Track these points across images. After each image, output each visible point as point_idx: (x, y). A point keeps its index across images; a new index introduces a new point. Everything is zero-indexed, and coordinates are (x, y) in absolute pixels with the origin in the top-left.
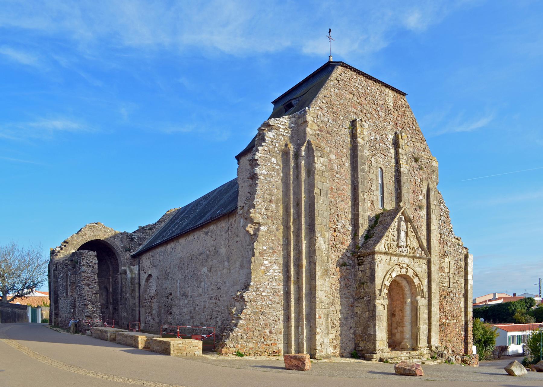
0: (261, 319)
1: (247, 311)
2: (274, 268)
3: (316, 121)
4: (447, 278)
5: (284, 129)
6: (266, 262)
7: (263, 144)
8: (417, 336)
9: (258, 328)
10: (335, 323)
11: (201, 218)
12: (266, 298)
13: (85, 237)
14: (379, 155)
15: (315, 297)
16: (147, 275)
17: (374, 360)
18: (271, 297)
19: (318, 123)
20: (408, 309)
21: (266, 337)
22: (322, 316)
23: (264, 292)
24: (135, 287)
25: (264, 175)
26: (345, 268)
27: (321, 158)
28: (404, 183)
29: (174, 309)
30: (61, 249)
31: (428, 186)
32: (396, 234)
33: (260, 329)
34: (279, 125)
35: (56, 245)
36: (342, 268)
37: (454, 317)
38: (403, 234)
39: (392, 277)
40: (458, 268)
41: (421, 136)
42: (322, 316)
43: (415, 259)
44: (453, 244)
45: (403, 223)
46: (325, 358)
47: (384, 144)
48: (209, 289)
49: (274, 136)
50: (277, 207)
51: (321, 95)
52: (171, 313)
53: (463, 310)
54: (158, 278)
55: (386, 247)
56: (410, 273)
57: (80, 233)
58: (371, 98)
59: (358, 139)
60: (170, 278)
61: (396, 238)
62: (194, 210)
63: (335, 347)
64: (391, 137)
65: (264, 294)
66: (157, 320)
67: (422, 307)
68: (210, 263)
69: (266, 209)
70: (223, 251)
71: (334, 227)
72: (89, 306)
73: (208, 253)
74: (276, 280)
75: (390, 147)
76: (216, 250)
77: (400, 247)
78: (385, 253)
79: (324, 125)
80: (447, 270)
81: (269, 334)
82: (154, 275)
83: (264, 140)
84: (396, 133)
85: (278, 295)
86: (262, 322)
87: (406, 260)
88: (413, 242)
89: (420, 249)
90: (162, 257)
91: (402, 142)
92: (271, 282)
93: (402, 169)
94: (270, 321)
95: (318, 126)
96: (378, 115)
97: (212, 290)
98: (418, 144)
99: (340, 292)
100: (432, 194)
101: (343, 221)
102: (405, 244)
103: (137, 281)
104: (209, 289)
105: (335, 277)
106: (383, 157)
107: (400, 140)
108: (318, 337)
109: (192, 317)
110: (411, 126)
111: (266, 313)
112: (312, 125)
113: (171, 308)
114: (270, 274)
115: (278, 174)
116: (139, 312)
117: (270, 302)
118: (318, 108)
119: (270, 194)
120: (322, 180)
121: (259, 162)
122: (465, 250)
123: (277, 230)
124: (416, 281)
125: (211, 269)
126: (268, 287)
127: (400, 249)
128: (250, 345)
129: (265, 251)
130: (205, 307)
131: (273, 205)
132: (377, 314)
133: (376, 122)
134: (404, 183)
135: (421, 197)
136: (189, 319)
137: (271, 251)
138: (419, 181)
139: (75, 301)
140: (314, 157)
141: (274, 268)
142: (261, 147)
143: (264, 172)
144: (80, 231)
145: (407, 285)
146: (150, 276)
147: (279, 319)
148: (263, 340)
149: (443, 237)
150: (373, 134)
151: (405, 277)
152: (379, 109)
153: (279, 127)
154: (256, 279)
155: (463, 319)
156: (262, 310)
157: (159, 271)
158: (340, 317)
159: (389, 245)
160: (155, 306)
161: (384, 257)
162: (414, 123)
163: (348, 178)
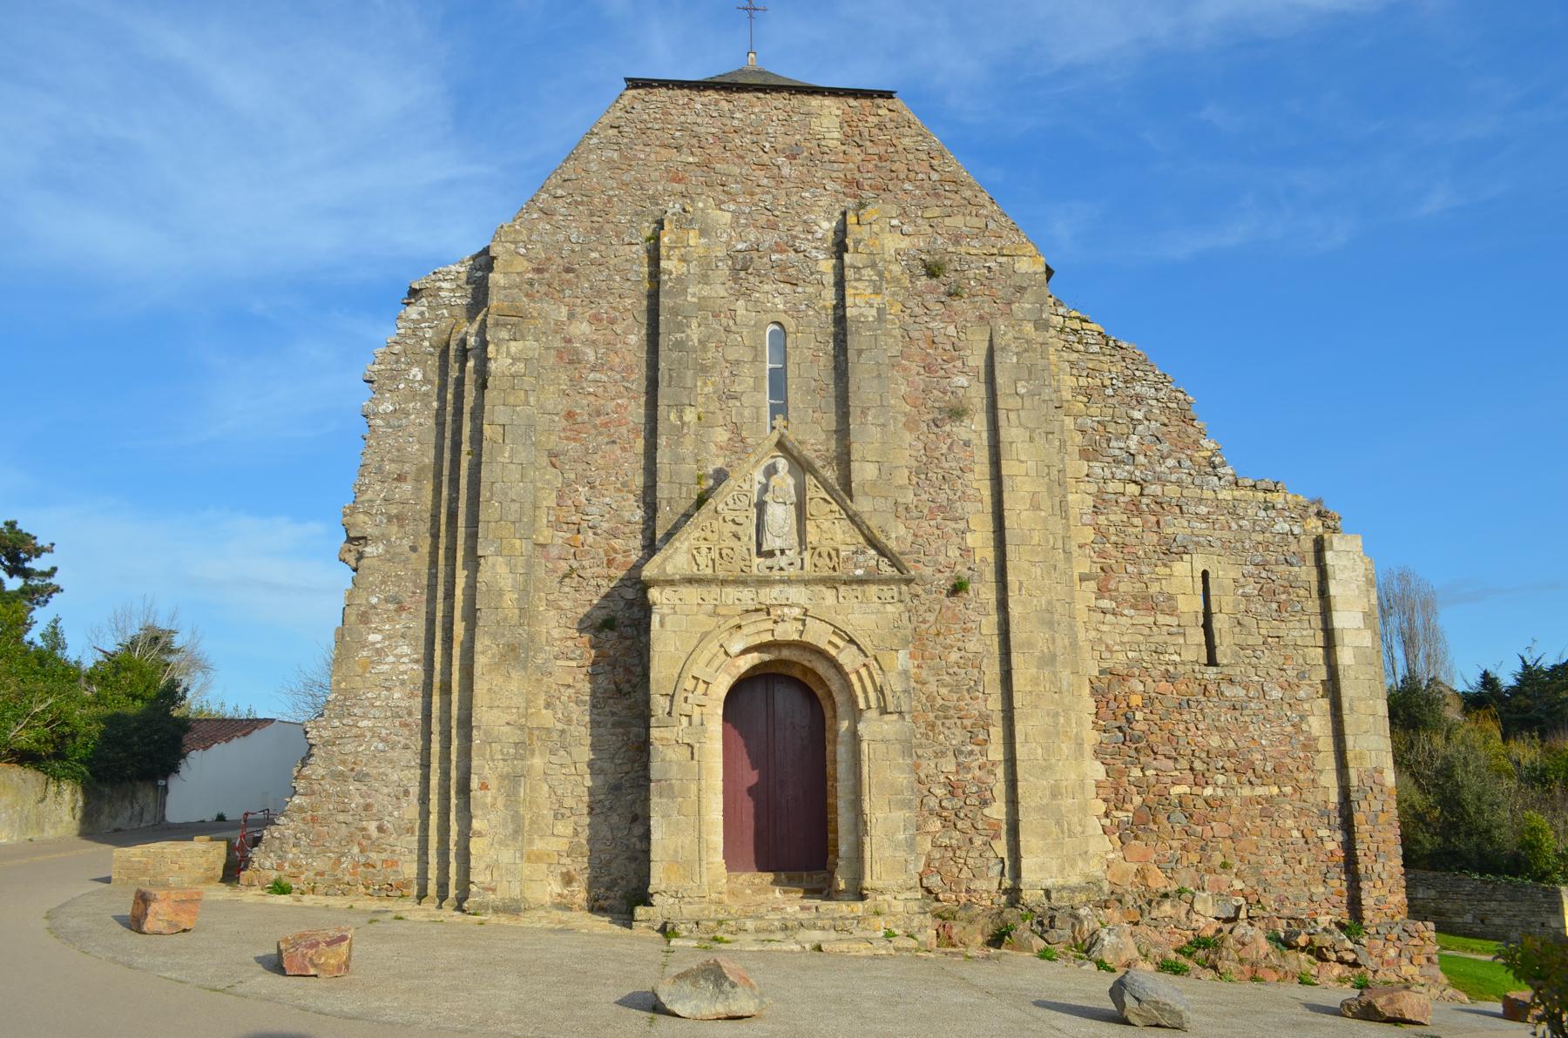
2: (398, 651)
5: (453, 290)
6: (373, 638)
10: (569, 802)
17: (639, 929)
22: (493, 783)
23: (364, 717)
26: (613, 635)
27: (513, 344)
28: (860, 352)
33: (349, 819)
36: (602, 636)
42: (493, 783)
43: (842, 589)
46: (496, 910)
49: (422, 314)
50: (417, 490)
56: (818, 635)
63: (568, 880)
64: (826, 227)
65: (363, 723)
74: (403, 683)
77: (771, 554)
78: (690, 581)
85: (406, 725)
86: (356, 801)
87: (798, 594)
89: (872, 552)
92: (388, 689)
94: (381, 799)
95: (530, 260)
96: (779, 180)
99: (594, 706)
100: (1006, 363)
105: (574, 664)
112: (508, 263)
114: (386, 667)
115: (427, 406)
117: (381, 746)
119: (399, 461)
123: (414, 549)
128: (318, 864)
129: (374, 607)
131: (407, 487)
132: (654, 774)
137: (392, 607)
138: (951, 330)
141: (398, 651)
147: (406, 793)
148: (356, 850)
153: (440, 289)
154: (343, 685)
156: (358, 768)
158: (589, 783)
161: (691, 594)
163: (634, 377)
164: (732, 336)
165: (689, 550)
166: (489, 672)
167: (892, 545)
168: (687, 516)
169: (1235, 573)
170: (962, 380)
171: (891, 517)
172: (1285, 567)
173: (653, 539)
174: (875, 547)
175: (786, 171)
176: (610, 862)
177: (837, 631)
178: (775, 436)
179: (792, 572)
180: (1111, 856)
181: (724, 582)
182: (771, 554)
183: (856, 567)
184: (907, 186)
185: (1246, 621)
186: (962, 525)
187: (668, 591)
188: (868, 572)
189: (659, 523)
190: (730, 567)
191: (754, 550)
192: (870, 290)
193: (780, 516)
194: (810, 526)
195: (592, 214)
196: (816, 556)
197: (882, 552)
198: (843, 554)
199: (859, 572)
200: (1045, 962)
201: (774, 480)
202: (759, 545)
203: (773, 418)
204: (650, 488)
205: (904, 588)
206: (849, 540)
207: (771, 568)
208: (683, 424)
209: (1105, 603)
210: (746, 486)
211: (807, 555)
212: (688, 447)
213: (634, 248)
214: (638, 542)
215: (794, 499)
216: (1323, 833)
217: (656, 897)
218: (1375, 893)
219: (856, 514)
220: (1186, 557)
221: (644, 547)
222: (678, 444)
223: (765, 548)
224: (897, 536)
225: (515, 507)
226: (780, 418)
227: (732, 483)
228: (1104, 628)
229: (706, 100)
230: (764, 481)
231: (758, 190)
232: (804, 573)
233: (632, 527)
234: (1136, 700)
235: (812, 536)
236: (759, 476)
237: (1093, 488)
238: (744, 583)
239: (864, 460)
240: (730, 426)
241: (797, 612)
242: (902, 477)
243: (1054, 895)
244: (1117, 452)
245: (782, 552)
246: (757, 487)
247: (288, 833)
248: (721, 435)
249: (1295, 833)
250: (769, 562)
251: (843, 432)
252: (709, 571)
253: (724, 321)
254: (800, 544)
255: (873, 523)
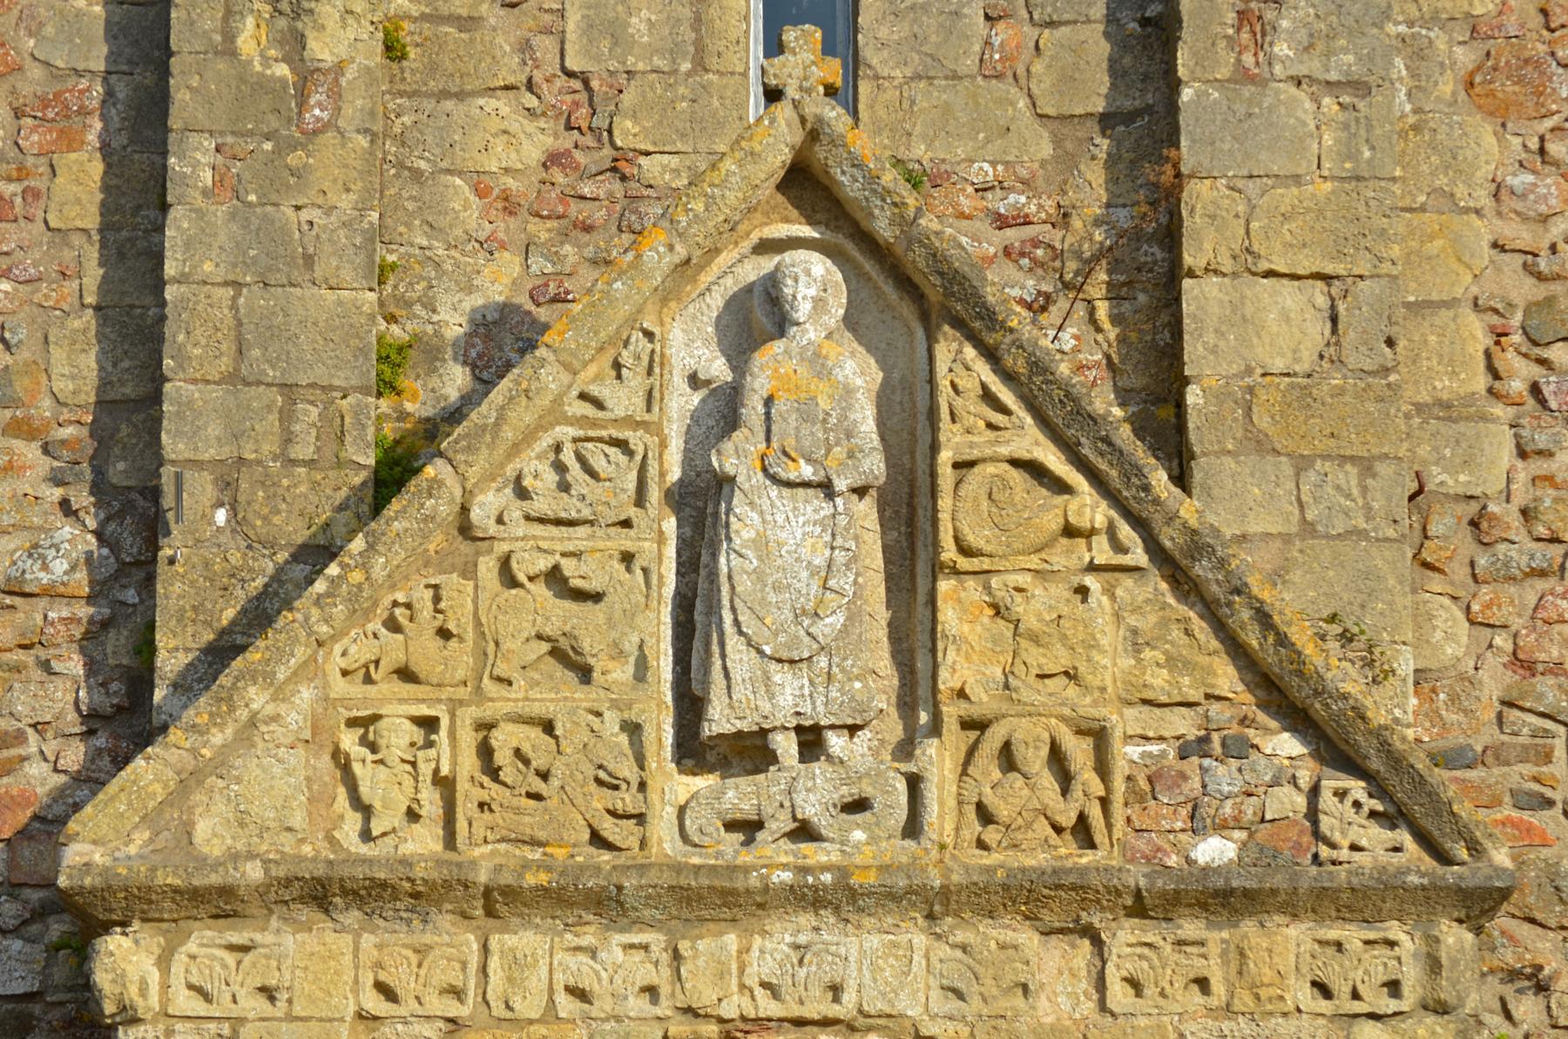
43: (1124, 936)
77: (750, 751)
78: (320, 893)
89: (1287, 745)
123: (413, 816)
165: (316, 735)
167: (1397, 711)
168: (318, 553)
171: (1392, 564)
173: (140, 678)
174: (1298, 719)
178: (778, 142)
179: (860, 846)
181: (498, 902)
182: (750, 751)
183: (1198, 825)
187: (203, 944)
188: (1258, 854)
189: (172, 590)
190: (532, 820)
191: (662, 731)
193: (798, 548)
194: (958, 606)
196: (987, 766)
197: (1335, 746)
198: (1128, 754)
199: (1215, 850)
201: (772, 366)
202: (690, 705)
203: (774, 47)
204: (131, 405)
205: (1454, 937)
206: (1159, 681)
207: (749, 828)
208: (307, 75)
210: (623, 399)
211: (938, 759)
212: (330, 194)
214: (64, 689)
215: (875, 466)
219: (1197, 545)
221: (93, 721)
222: (283, 179)
223: (719, 720)
224: (1422, 666)
226: (804, 40)
227: (551, 378)
230: (718, 369)
232: (923, 851)
233: (30, 615)
235: (968, 661)
236: (691, 345)
238: (607, 905)
239: (1251, 266)
240: (556, 92)
242: (1452, 358)
245: (811, 741)
246: (682, 403)
248: (512, 140)
250: (740, 794)
251: (1144, 122)
252: (424, 842)
254: (907, 704)
255: (1296, 604)
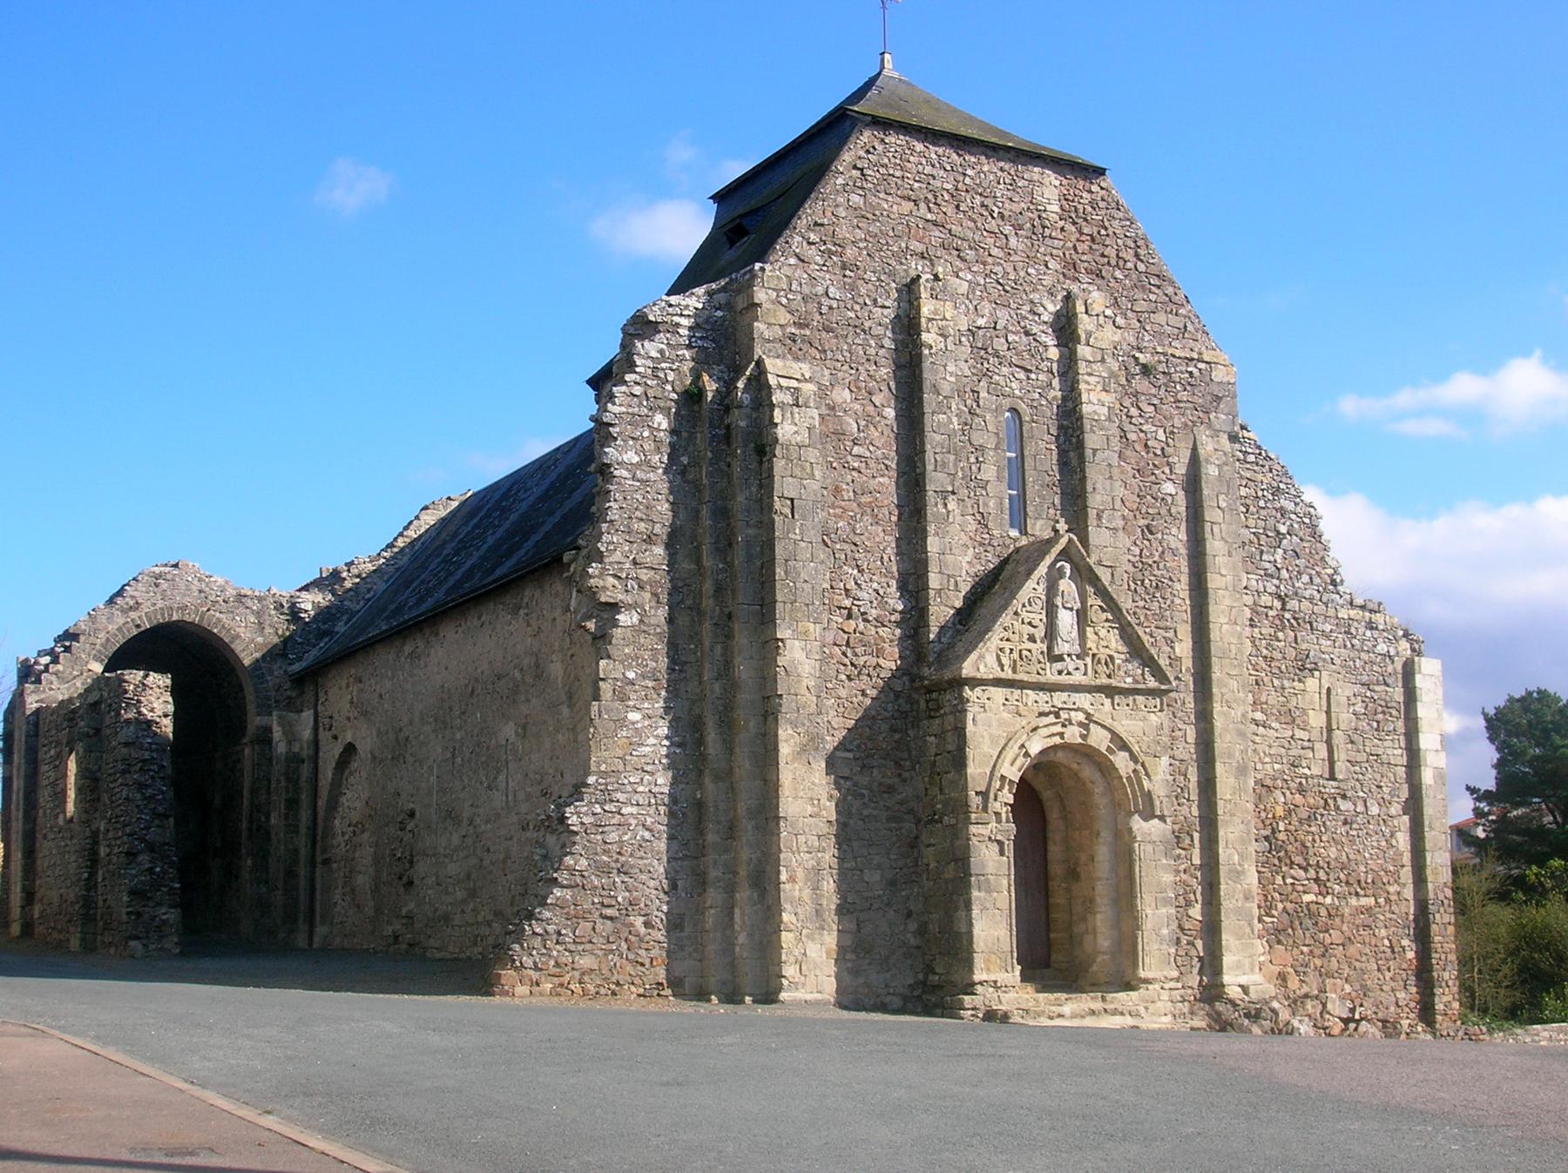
0: (619, 884)
1: (578, 861)
3: (784, 301)
4: (1322, 751)
6: (633, 716)
7: (628, 377)
8: (1135, 945)
9: (609, 912)
11: (508, 555)
12: (633, 822)
13: (133, 615)
14: (1005, 370)
15: (778, 818)
16: (338, 749)
18: (649, 820)
19: (794, 305)
20: (1103, 853)
21: (632, 938)
22: (800, 874)
23: (629, 803)
24: (297, 790)
25: (632, 468)
29: (422, 867)
30: (55, 660)
31: (1194, 449)
32: (1039, 617)
34: (676, 319)
35: (34, 641)
37: (1356, 886)
38: (1066, 620)
39: (1027, 754)
40: (1375, 711)
41: (1170, 290)
42: (800, 874)
44: (1347, 628)
45: (1067, 586)
47: (1027, 334)
48: (521, 796)
49: (661, 352)
51: (802, 223)
52: (410, 883)
53: (1407, 858)
54: (374, 758)
55: (1005, 661)
56: (1099, 739)
57: (119, 600)
58: (978, 200)
59: (925, 336)
60: (410, 759)
61: (1040, 633)
62: (505, 511)
66: (369, 910)
67: (1149, 848)
68: (524, 709)
69: (635, 562)
70: (556, 669)
71: (847, 603)
72: (140, 858)
73: (517, 674)
75: (1050, 340)
76: (537, 665)
77: (1060, 658)
78: (998, 682)
79: (813, 307)
80: (1317, 720)
81: (643, 930)
82: (364, 748)
83: (631, 367)
84: (1069, 298)
87: (1083, 700)
88: (1106, 640)
90: (388, 684)
91: (1085, 324)
93: (1086, 409)
96: (1006, 248)
97: (529, 797)
98: (1160, 318)
101: (875, 585)
102: (1077, 649)
103: (305, 770)
104: (521, 796)
105: (850, 755)
106: (1022, 375)
107: (1083, 317)
108: (786, 938)
109: (473, 894)
110: (1129, 265)
111: (632, 867)
113: (411, 862)
116: (312, 881)
117: (647, 835)
118: (792, 261)
120: (797, 472)
121: (614, 431)
122: (1404, 645)
124: (1121, 761)
125: (524, 727)
126: (641, 789)
127: (1059, 665)
130: (508, 857)
133: (997, 269)
134: (1095, 451)
135: (1169, 488)
136: (464, 901)
138: (1161, 435)
139: (96, 843)
140: (772, 406)
142: (623, 388)
143: (632, 457)
144: (120, 593)
145: (1097, 776)
146: (350, 749)
148: (624, 946)
149: (1293, 604)
150: (986, 308)
151: (1085, 752)
152: (1008, 229)
153: (678, 325)
155: (1409, 893)
157: (379, 733)
159: (1016, 655)
160: (365, 856)
161: (998, 693)
162: (1142, 252)
164: (976, 420)
166: (793, 761)
169: (1349, 693)
170: (1169, 488)
172: (1383, 687)
175: (1013, 241)
176: (887, 958)
177: (1116, 738)
180: (1262, 958)
184: (1118, 274)
185: (1355, 738)
186: (1170, 634)
192: (1100, 387)
195: (844, 268)
200: (1277, 1039)
209: (1259, 716)
213: (886, 312)
216: (1405, 942)
217: (979, 987)
218: (1445, 999)
220: (1317, 674)
225: (807, 587)
228: (1258, 739)
229: (940, 151)
231: (990, 260)
234: (1280, 811)
237: (1249, 600)
241: (1081, 717)
243: (1252, 989)
244: (1267, 565)
247: (551, 928)
249: (1386, 942)
253: (969, 402)
